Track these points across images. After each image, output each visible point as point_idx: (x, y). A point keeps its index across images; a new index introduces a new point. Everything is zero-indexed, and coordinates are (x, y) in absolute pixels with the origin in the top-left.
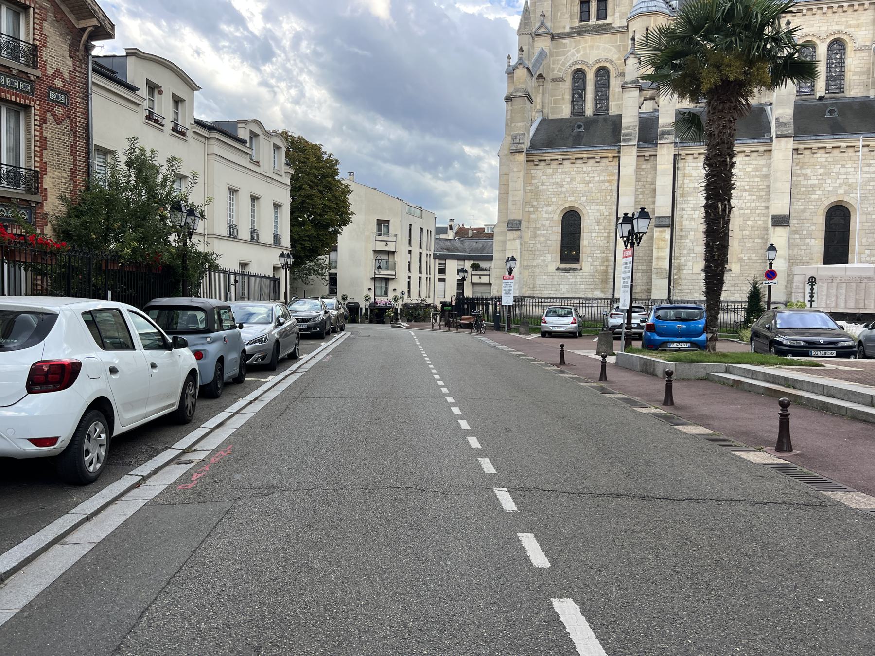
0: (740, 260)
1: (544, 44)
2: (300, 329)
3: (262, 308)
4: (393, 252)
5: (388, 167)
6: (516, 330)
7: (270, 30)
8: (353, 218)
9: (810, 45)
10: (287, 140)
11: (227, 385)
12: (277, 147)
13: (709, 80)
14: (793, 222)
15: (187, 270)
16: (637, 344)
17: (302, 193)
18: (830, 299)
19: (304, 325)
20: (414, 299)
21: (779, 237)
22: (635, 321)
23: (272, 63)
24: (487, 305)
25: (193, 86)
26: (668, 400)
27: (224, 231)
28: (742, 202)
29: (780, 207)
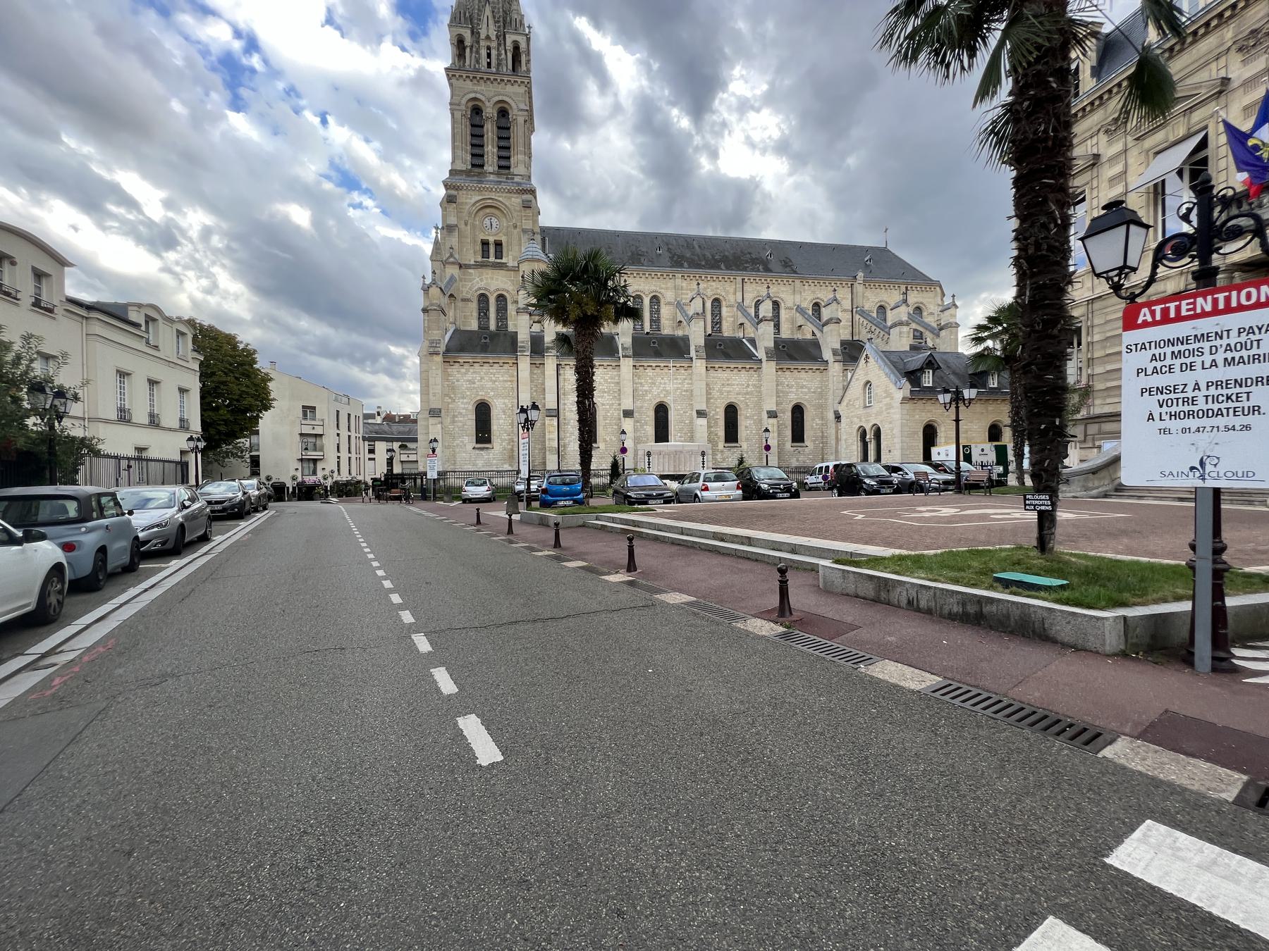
0: (605, 441)
1: (453, 271)
2: (212, 511)
3: (161, 493)
4: (321, 435)
5: (314, 359)
6: (441, 499)
7: (172, 219)
8: (275, 403)
9: (638, 298)
10: (195, 328)
11: (112, 576)
12: (180, 334)
13: (575, 313)
14: (636, 414)
15: (55, 455)
16: (536, 504)
17: (215, 379)
18: (661, 465)
19: (219, 507)
20: (344, 477)
21: (628, 424)
22: (533, 488)
23: (176, 251)
24: (415, 479)
25: (62, 262)
26: (557, 544)
27: (113, 415)
28: (601, 399)
29: (627, 404)
